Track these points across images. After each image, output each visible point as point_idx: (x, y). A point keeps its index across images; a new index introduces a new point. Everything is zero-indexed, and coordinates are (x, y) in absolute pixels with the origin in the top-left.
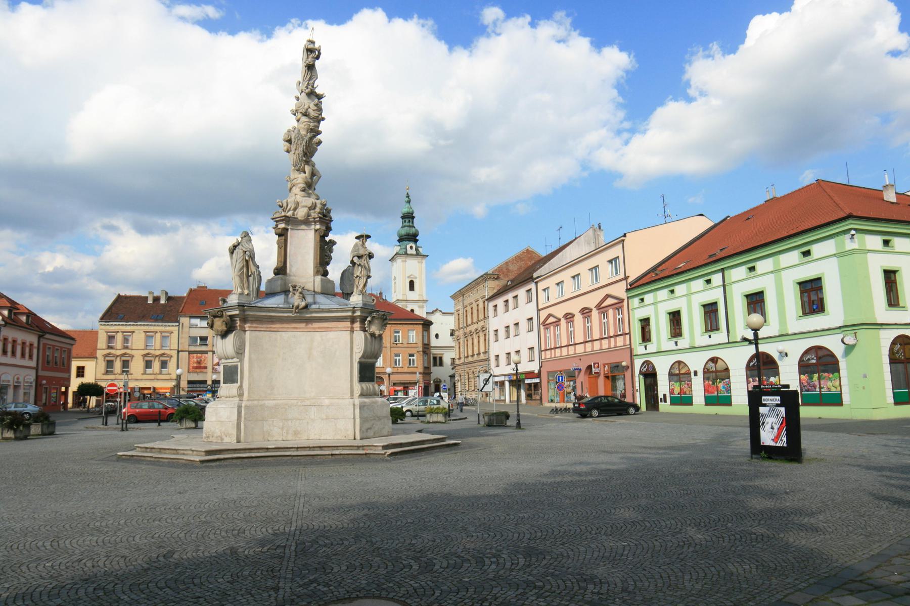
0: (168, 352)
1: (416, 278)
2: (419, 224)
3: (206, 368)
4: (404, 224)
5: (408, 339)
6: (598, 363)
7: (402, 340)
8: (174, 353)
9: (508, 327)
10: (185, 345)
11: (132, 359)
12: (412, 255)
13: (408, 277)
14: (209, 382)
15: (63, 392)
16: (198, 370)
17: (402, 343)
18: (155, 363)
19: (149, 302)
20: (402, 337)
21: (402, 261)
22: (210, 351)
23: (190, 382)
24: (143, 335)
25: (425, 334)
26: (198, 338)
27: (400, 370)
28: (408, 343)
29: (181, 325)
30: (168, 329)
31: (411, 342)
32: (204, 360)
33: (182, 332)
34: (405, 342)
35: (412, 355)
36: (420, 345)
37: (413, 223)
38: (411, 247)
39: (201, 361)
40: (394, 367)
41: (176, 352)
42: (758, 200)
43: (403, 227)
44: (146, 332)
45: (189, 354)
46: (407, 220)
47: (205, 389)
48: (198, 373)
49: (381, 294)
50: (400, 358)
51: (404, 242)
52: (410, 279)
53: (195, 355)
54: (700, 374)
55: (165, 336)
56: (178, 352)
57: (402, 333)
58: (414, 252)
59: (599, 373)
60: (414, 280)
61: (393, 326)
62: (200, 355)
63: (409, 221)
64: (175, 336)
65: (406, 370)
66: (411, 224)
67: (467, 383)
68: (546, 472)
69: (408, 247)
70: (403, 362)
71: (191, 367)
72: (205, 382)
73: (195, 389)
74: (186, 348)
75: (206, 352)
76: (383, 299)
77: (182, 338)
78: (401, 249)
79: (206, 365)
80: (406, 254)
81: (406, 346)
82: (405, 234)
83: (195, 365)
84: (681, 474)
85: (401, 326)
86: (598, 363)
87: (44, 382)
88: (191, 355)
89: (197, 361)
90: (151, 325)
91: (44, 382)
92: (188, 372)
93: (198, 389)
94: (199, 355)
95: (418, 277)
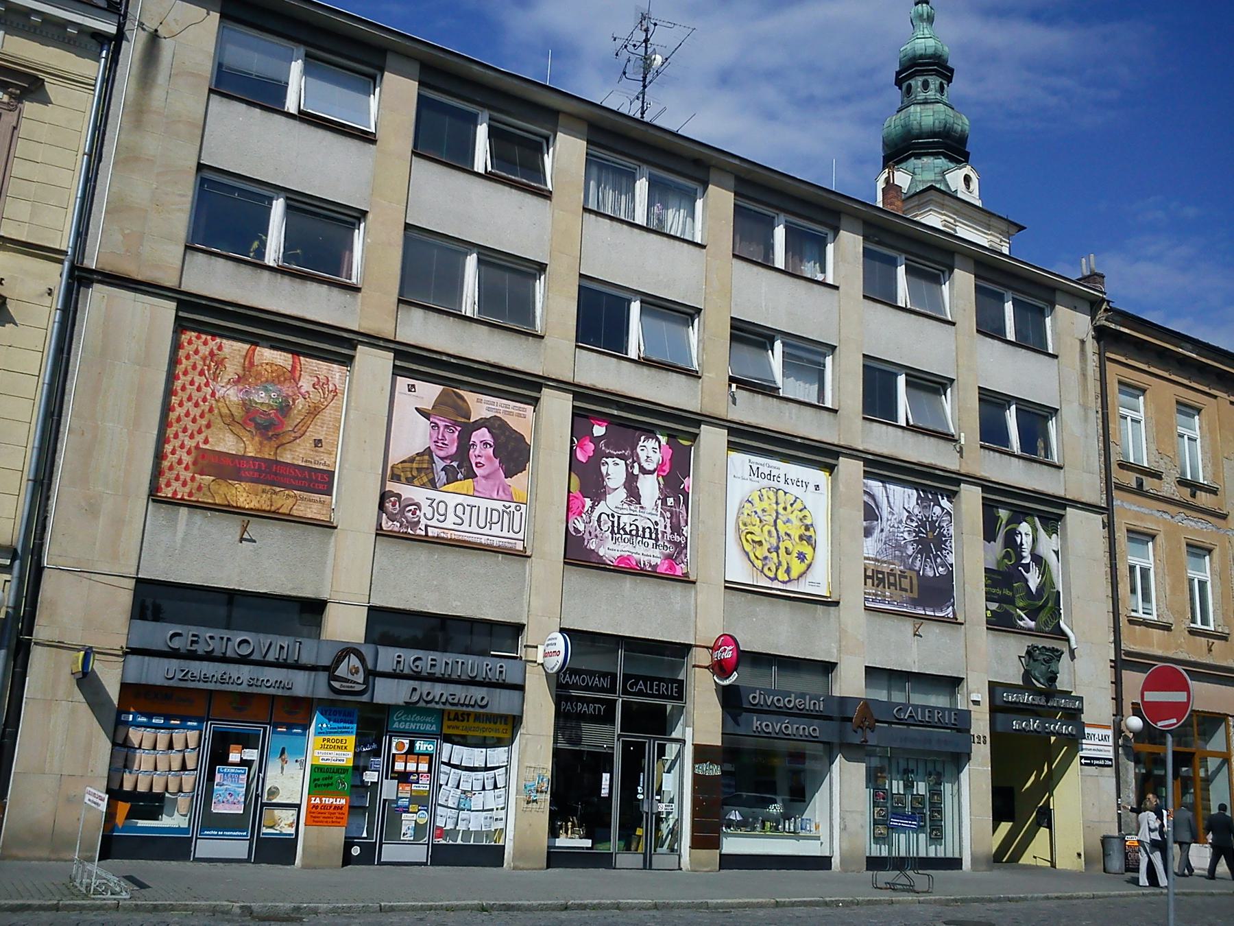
9: (1083, 342)
22: (374, 341)
29: (131, 51)
32: (314, 412)
33: (139, 112)
39: (285, 408)
41: (55, 275)
42: (1225, 349)
45: (181, 325)
47: (301, 684)
53: (233, 349)
62: (282, 359)
68: (1083, 413)
71: (179, 454)
77: (128, 159)
79: (321, 461)
82: (938, 126)
83: (227, 443)
87: (921, 788)
88: (198, 345)
91: (921, 788)
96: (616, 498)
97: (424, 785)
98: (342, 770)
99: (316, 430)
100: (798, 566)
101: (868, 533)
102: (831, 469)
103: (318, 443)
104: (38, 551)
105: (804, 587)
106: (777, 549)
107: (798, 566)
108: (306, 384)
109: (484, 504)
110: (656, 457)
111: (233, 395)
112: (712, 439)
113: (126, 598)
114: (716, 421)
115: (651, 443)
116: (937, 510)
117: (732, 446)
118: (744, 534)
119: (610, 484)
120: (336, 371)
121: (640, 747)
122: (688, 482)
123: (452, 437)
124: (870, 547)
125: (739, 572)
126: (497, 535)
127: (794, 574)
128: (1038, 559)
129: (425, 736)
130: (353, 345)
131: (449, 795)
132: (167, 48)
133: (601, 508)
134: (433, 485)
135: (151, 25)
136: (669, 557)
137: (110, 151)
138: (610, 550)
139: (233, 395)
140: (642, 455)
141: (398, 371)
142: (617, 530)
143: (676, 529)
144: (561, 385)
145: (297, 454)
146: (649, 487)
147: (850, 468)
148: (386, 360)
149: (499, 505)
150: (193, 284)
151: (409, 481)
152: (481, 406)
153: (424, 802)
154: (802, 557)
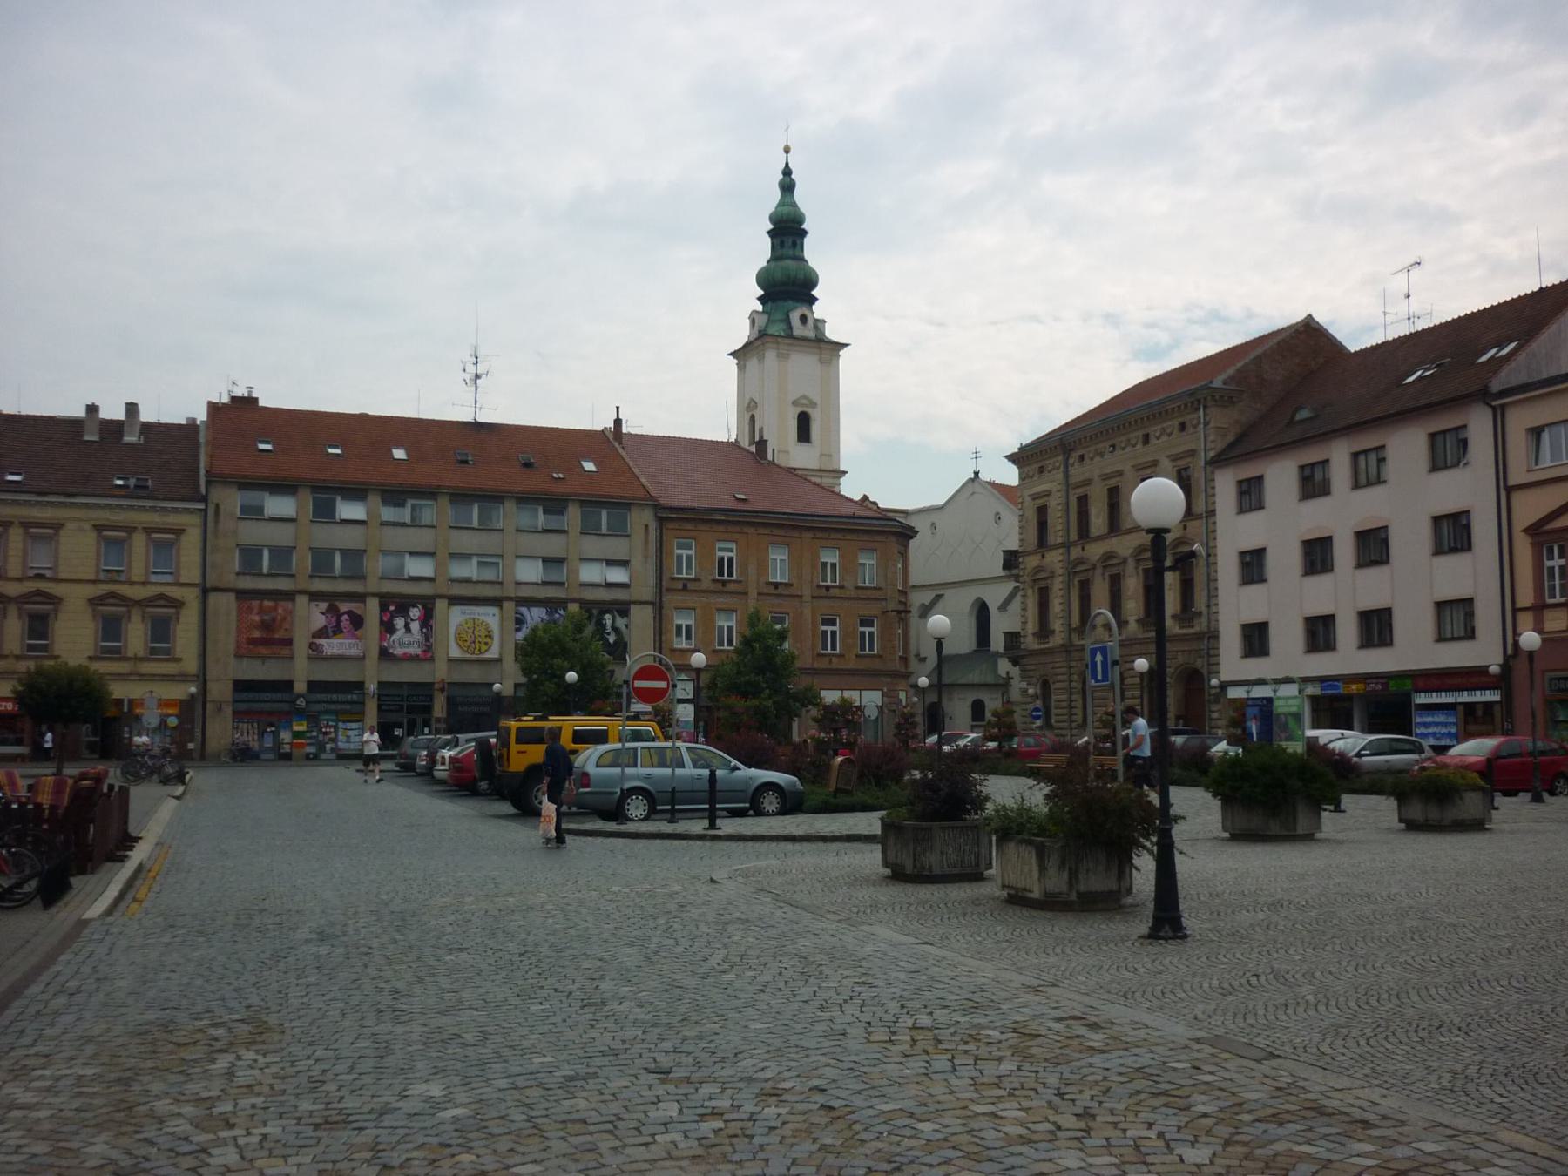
0: (175, 592)
1: (814, 405)
2: (815, 253)
3: (288, 642)
4: (780, 252)
7: (842, 579)
8: (191, 596)
9: (647, 526)
10: (229, 567)
11: (178, 613)
12: (805, 339)
13: (795, 403)
14: (300, 687)
15: (186, 746)
16: (264, 651)
17: (841, 587)
18: (131, 626)
19: (87, 438)
22: (441, 597)
23: (241, 686)
24: (90, 538)
26: (266, 554)
27: (836, 664)
28: (858, 588)
30: (173, 520)
31: (867, 584)
32: (284, 619)
35: (867, 622)
39: (274, 620)
40: (715, 651)
44: (98, 528)
47: (285, 707)
48: (264, 658)
50: (874, 629)
52: (800, 409)
53: (255, 603)
55: (165, 543)
56: (205, 591)
60: (809, 410)
61: (820, 535)
64: (192, 539)
67: (1079, 704)
70: (843, 640)
72: (288, 685)
73: (257, 706)
74: (231, 580)
75: (290, 596)
80: (790, 335)
81: (853, 594)
83: (257, 634)
84: (39, 754)
85: (839, 536)
89: (263, 622)
90: (120, 507)
93: (267, 707)
94: (267, 603)
96: (401, 631)
97: (333, 735)
98: (1497, 702)
99: (286, 626)
100: (484, 648)
101: (518, 630)
102: (500, 606)
103: (286, 630)
104: (204, 675)
105: (488, 656)
106: (474, 642)
107: (484, 648)
108: (280, 611)
109: (347, 641)
110: (418, 614)
111: (257, 618)
112: (440, 605)
113: (231, 686)
114: (441, 597)
115: (416, 609)
116: (557, 616)
117: (311, 600)
118: (458, 638)
119: (398, 627)
120: (289, 605)
121: (414, 720)
122: (432, 622)
123: (334, 619)
124: (520, 636)
125: (455, 652)
126: (353, 652)
127: (483, 650)
128: (615, 629)
129: (332, 720)
130: (294, 595)
131: (341, 737)
132: (222, 507)
133: (394, 636)
134: (328, 637)
135: (215, 501)
136: (425, 651)
137: (209, 548)
138: (398, 651)
139: (257, 618)
140: (411, 614)
141: (311, 600)
142: (401, 644)
143: (427, 639)
144: (374, 595)
145: (278, 635)
146: (415, 626)
147: (507, 605)
148: (445, 602)
149: (353, 641)
150: (384, 590)
151: (320, 637)
152: (344, 607)
153: (334, 740)
154: (486, 644)
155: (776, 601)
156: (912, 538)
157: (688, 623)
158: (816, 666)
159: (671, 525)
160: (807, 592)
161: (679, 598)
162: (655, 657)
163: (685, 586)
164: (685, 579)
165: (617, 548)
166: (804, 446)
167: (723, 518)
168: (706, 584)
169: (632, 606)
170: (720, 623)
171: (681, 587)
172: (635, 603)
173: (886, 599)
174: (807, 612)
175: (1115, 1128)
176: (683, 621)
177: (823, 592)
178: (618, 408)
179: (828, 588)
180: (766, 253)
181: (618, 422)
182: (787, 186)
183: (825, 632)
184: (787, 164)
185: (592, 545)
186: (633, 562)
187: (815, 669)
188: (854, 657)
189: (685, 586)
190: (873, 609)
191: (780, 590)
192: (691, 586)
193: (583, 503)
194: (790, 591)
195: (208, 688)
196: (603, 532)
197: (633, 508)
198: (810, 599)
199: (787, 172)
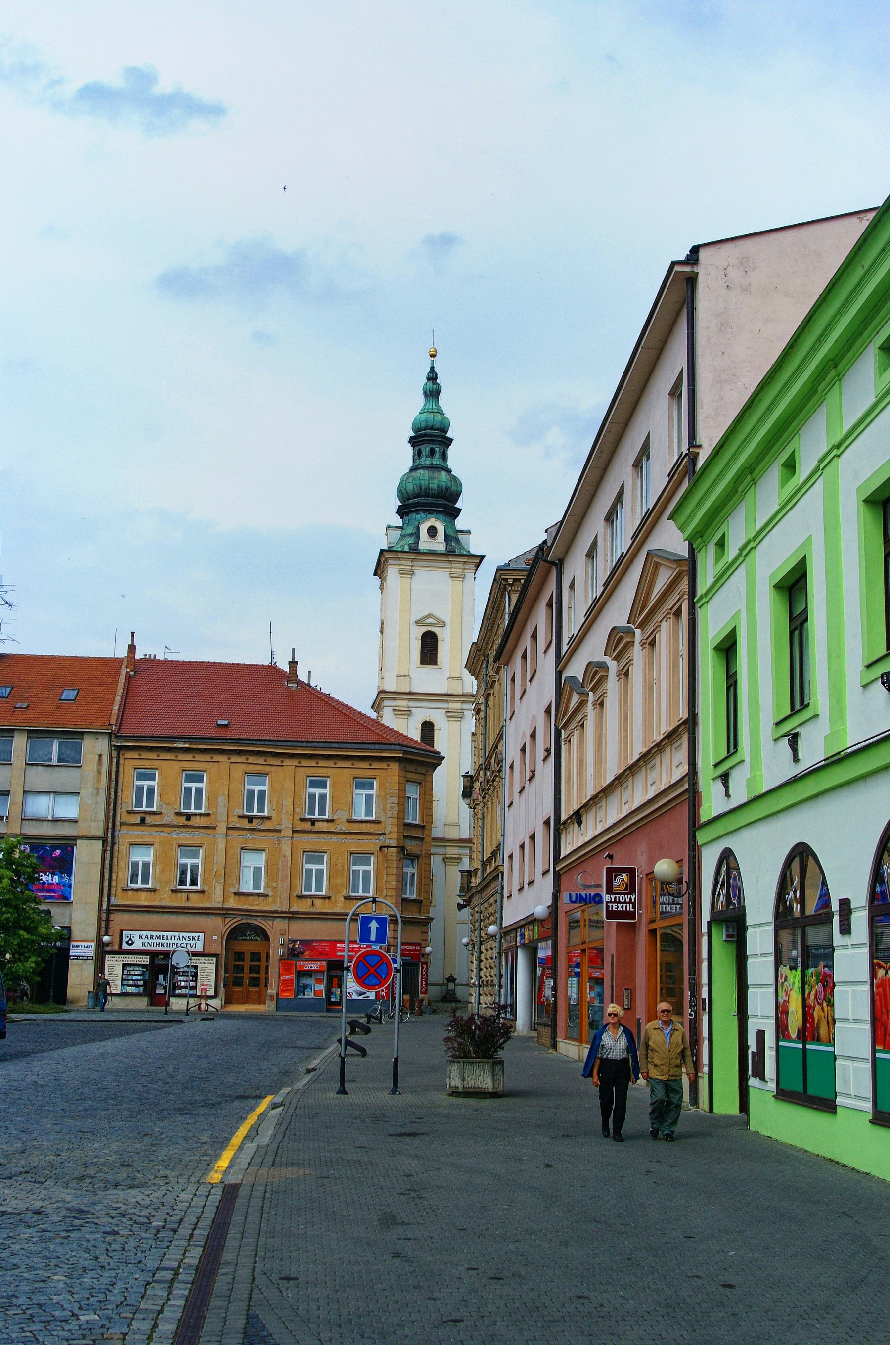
1: (443, 625)
5: (350, 810)
6: (631, 872)
7: (333, 811)
9: (100, 756)
13: (418, 623)
20: (333, 797)
21: (401, 573)
25: (413, 792)
27: (320, 906)
28: (350, 821)
34: (341, 816)
36: (390, 827)
37: (444, 457)
38: (432, 531)
43: (413, 469)
46: (426, 449)
49: (293, 664)
51: (414, 516)
54: (860, 920)
57: (333, 786)
58: (439, 545)
59: (631, 915)
61: (305, 763)
63: (432, 452)
65: (166, 899)
66: (437, 461)
69: (424, 528)
76: (299, 682)
78: (403, 536)
80: (415, 550)
81: (344, 827)
85: (330, 763)
86: (631, 872)
92: (566, 912)
95: (447, 620)
155: (249, 835)
156: (434, 766)
157: (146, 859)
158: (294, 908)
159: (129, 755)
160: (286, 825)
161: (136, 834)
162: (351, 919)
163: (143, 820)
164: (146, 813)
165: (65, 777)
166: (429, 669)
167: (187, 746)
168: (169, 818)
169: (79, 842)
170: (134, 858)
171: (139, 821)
172: (82, 838)
173: (384, 834)
174: (286, 849)
175: (40, 1308)
176: (142, 856)
177: (307, 826)
178: (133, 633)
179: (313, 822)
180: (408, 462)
181: (132, 648)
182: (433, 393)
183: (309, 871)
184: (432, 368)
185: (39, 777)
186: (82, 792)
187: (293, 913)
188: (342, 899)
189: (143, 820)
190: (372, 844)
191: (255, 824)
192: (149, 820)
193: (32, 734)
194: (267, 825)
195: (127, 998)
196: (55, 764)
197: (85, 736)
198: (289, 833)
199: (432, 377)
